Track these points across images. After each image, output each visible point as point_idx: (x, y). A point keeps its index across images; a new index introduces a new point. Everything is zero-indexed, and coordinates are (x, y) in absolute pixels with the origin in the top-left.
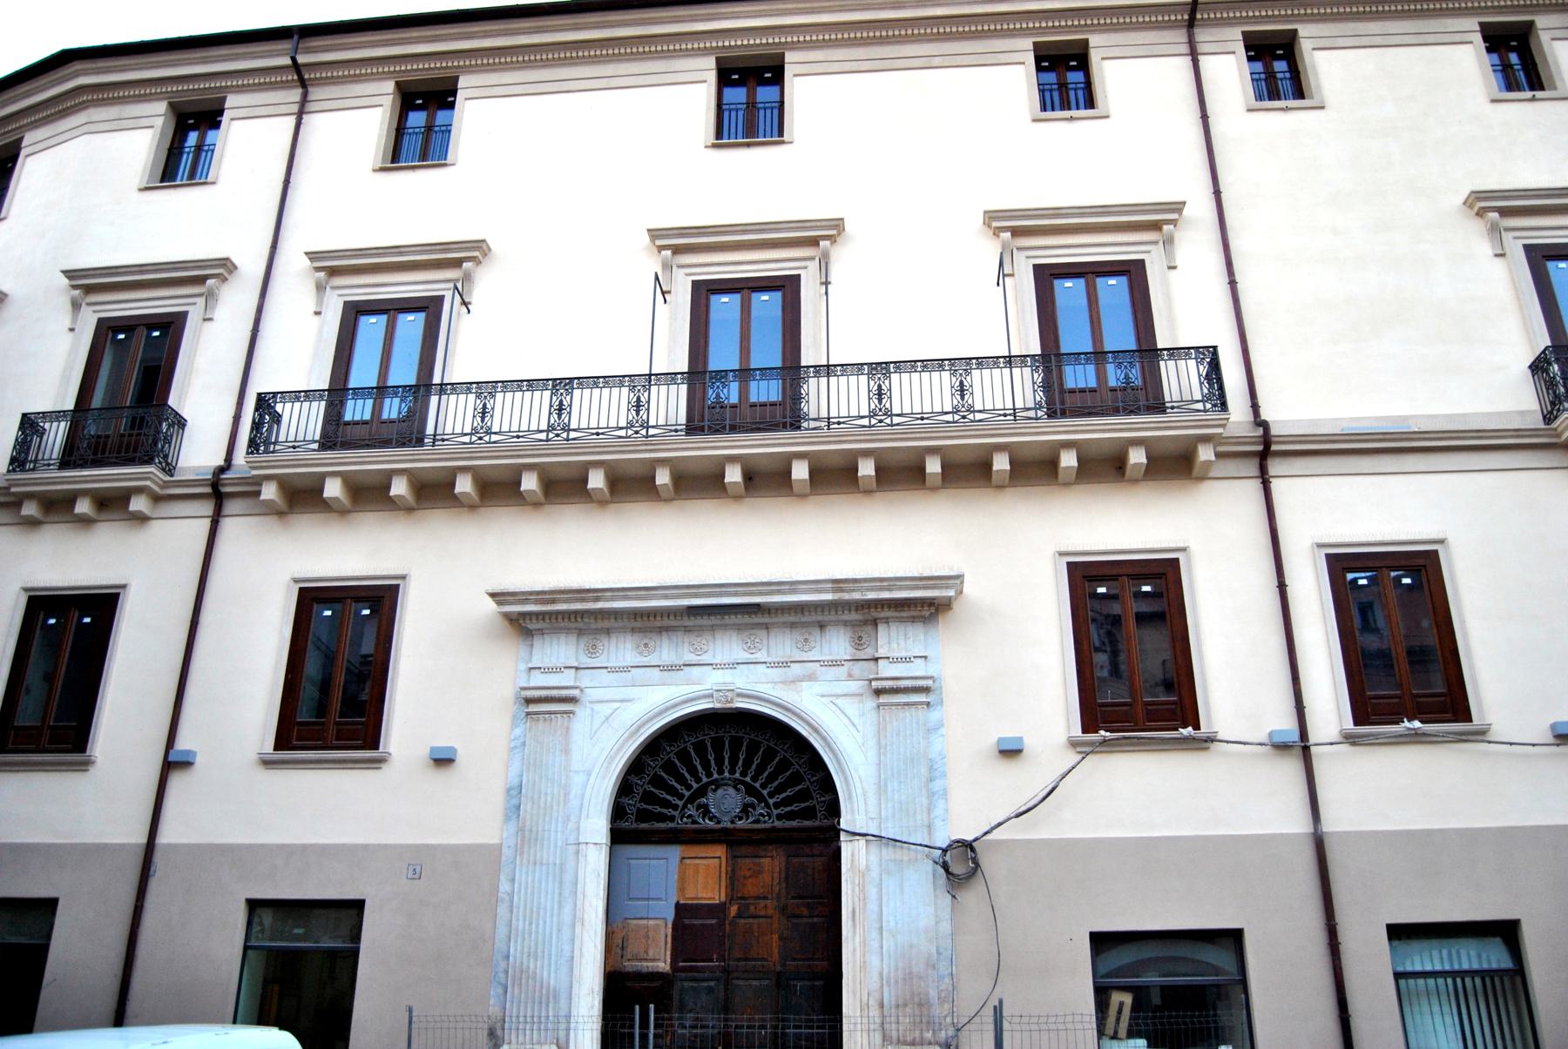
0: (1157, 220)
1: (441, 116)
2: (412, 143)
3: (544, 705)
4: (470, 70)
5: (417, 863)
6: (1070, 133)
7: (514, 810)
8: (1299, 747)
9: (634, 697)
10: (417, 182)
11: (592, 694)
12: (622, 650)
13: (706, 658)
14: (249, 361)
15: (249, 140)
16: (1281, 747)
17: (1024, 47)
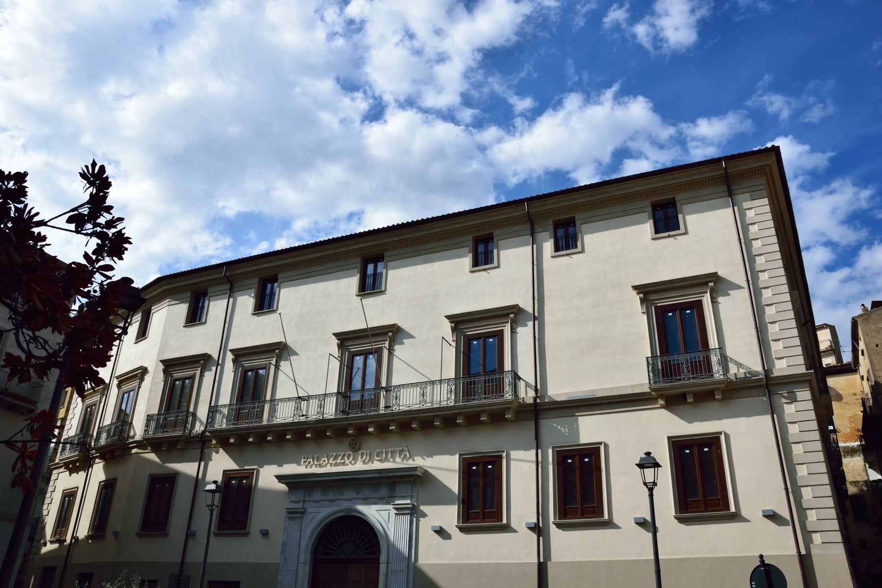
0: (713, 283)
1: (571, 229)
2: (481, 258)
3: (295, 514)
4: (213, 285)
5: (256, 569)
6: (669, 244)
7: (283, 551)
8: (649, 525)
9: (322, 511)
10: (371, 302)
11: (309, 510)
12: (318, 495)
13: (343, 497)
14: (308, 383)
15: (216, 308)
16: (642, 523)
17: (647, 203)
